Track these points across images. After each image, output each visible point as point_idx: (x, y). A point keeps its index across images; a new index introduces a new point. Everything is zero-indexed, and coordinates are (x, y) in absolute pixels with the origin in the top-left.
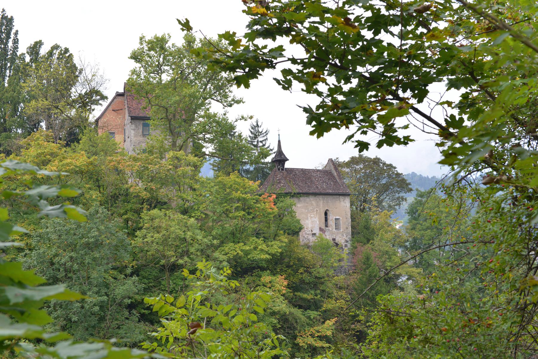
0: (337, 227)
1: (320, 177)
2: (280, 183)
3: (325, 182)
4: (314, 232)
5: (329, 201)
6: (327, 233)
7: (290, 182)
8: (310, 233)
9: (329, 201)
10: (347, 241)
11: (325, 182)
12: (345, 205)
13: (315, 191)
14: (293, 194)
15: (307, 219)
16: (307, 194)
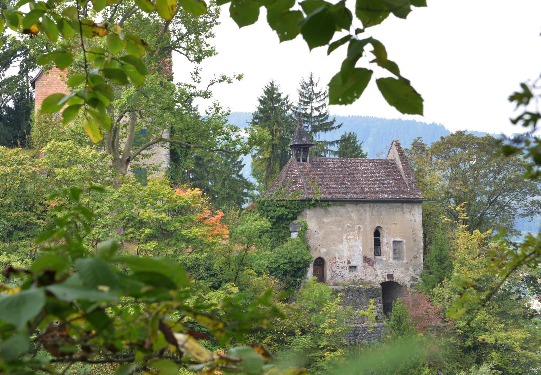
0: (397, 254)
1: (372, 172)
2: (296, 182)
3: (380, 181)
4: (353, 264)
5: (383, 213)
6: (376, 266)
7: (313, 182)
8: (346, 265)
9: (383, 213)
10: (414, 279)
11: (380, 181)
12: (413, 218)
13: (355, 196)
14: (313, 202)
15: (341, 242)
16: (342, 202)
